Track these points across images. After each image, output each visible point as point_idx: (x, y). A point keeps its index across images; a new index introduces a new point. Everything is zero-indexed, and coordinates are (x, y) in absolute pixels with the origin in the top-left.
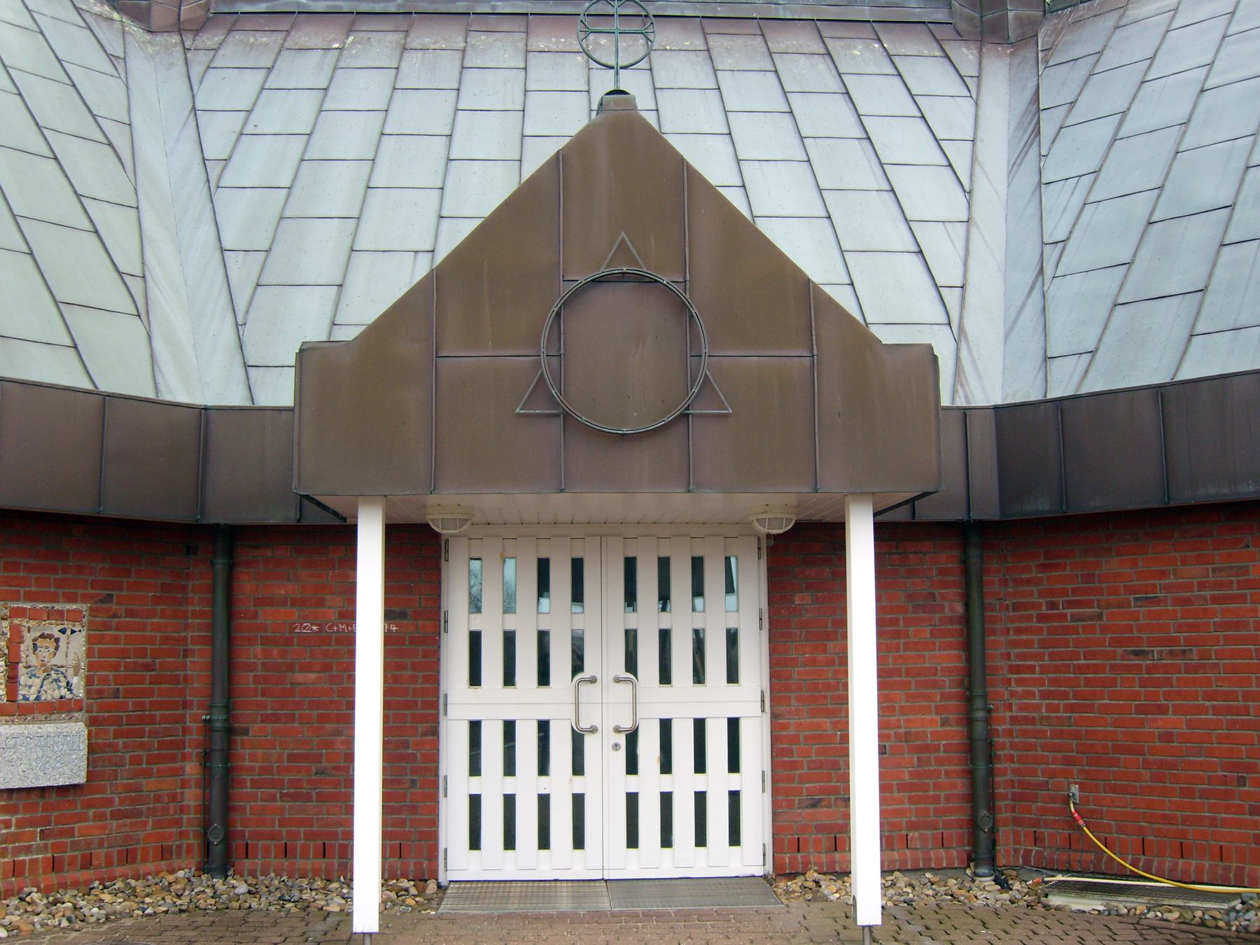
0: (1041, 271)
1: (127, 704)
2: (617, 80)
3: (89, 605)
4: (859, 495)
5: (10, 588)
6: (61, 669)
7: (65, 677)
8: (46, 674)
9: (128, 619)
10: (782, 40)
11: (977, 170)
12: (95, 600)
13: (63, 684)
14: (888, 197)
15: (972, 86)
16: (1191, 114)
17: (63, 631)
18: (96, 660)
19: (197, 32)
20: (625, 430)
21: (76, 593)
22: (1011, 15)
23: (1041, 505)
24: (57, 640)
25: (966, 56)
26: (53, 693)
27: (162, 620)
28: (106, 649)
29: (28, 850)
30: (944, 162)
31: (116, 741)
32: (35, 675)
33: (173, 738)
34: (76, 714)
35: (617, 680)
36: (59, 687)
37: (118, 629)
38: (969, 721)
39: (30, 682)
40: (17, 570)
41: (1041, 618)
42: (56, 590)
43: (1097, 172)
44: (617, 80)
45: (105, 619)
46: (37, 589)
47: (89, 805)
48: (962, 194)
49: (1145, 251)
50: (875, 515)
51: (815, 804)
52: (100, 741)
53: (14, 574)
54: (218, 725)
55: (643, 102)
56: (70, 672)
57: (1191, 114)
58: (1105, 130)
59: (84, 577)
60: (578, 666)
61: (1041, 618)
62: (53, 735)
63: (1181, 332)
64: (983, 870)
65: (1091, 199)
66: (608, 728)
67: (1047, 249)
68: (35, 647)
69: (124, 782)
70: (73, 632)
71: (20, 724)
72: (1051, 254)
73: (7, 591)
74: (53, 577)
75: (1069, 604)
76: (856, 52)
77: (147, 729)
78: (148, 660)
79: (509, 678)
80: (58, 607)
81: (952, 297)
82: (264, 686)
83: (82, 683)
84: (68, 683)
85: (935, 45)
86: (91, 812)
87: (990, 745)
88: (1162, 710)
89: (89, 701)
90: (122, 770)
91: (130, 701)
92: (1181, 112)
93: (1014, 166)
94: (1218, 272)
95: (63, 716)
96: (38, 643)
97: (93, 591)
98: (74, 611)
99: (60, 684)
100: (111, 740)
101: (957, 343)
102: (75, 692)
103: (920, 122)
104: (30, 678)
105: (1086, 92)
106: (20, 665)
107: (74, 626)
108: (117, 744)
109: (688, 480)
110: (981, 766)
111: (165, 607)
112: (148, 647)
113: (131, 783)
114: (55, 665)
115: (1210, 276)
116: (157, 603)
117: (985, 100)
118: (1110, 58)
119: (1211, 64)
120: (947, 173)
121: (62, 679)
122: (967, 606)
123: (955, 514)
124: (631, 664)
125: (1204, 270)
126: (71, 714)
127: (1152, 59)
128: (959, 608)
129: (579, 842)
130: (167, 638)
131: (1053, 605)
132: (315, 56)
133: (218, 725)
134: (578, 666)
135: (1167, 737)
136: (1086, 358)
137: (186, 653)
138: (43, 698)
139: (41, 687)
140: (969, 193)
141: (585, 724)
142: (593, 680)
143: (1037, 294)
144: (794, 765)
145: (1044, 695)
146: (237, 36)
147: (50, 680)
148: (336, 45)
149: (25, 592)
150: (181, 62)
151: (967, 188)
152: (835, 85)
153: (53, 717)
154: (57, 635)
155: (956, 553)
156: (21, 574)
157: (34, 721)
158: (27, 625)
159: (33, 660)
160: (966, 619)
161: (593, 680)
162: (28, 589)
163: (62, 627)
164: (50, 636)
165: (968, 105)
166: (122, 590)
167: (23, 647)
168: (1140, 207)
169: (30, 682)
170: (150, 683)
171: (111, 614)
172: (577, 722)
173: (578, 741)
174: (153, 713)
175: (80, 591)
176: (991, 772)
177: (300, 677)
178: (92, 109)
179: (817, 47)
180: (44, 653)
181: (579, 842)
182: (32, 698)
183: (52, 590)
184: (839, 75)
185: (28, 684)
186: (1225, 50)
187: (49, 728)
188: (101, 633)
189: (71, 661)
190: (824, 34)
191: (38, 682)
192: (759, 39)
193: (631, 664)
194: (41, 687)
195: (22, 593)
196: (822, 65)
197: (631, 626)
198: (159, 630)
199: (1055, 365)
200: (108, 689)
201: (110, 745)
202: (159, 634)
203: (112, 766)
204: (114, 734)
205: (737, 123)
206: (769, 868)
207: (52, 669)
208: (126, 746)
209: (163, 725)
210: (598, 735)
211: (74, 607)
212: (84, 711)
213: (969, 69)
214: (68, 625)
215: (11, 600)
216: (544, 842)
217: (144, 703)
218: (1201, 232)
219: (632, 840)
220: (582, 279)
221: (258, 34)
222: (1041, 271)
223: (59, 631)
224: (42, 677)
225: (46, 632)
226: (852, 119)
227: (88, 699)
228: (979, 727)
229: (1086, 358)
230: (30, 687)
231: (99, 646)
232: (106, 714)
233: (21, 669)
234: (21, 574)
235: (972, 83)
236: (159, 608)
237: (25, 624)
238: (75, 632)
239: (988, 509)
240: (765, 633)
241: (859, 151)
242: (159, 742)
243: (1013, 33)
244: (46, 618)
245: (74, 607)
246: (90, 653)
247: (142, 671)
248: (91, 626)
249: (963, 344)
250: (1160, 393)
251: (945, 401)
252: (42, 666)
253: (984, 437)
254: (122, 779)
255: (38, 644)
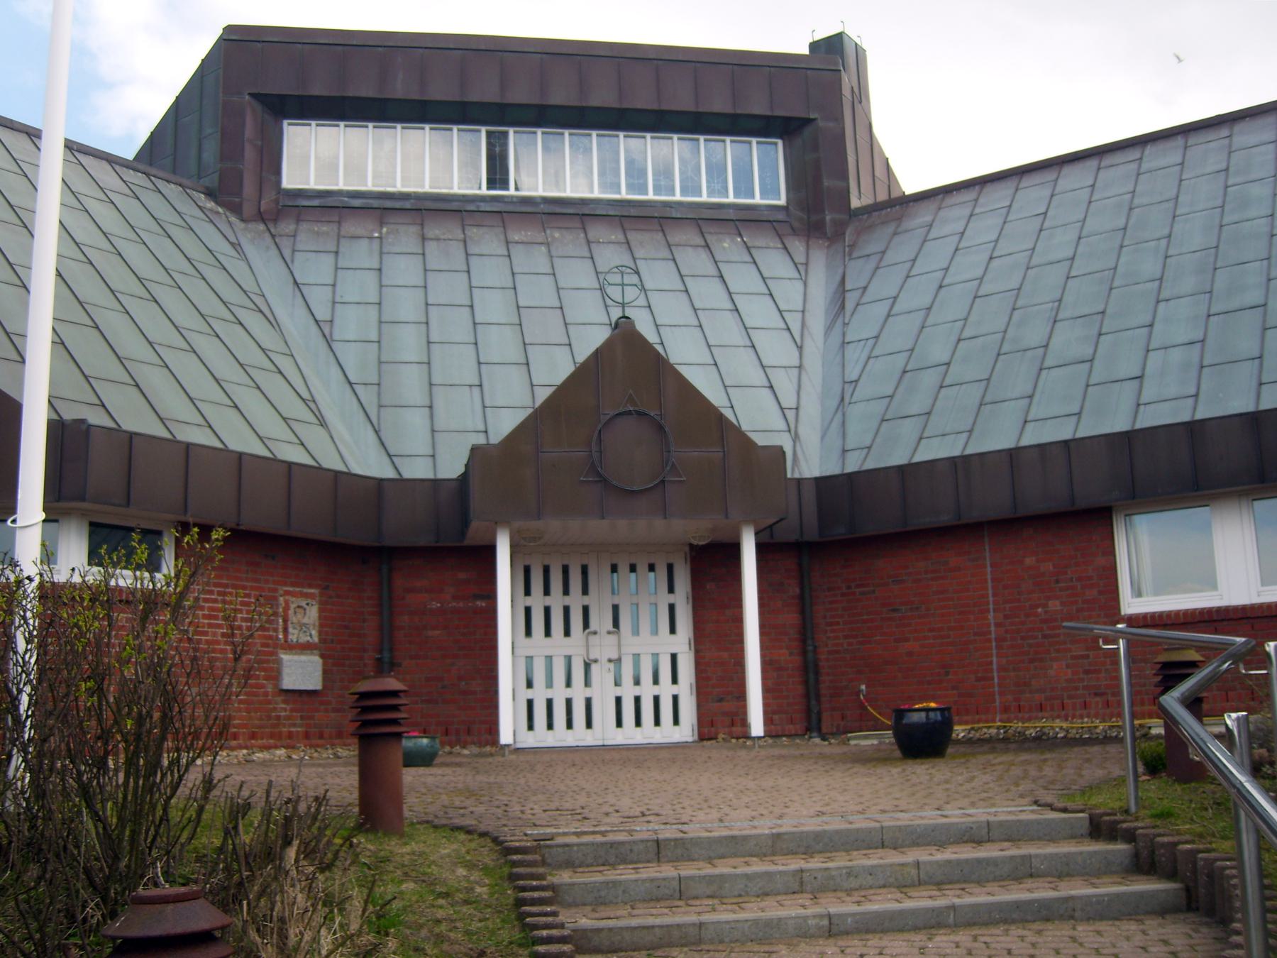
0: (842, 399)
2: (624, 311)
4: (747, 522)
10: (677, 236)
11: (806, 332)
14: (751, 351)
15: (802, 270)
16: (933, 303)
19: (275, 220)
20: (635, 488)
22: (828, 218)
23: (840, 531)
25: (797, 246)
26: (304, 639)
29: (294, 725)
30: (785, 327)
35: (609, 633)
38: (804, 653)
41: (843, 595)
43: (877, 337)
44: (624, 311)
47: (322, 703)
48: (795, 348)
49: (901, 389)
50: (756, 534)
51: (721, 700)
54: (386, 660)
55: (645, 328)
57: (933, 303)
58: (882, 308)
60: (586, 625)
61: (843, 595)
63: (915, 436)
64: (814, 734)
65: (873, 355)
66: (604, 660)
67: (846, 386)
68: (295, 612)
72: (849, 389)
75: (858, 586)
76: (726, 245)
79: (548, 633)
81: (791, 415)
85: (777, 239)
86: (323, 707)
87: (816, 666)
88: (907, 640)
92: (927, 301)
93: (829, 330)
94: (938, 403)
101: (794, 442)
103: (768, 298)
105: (874, 280)
109: (665, 512)
110: (812, 676)
115: (933, 405)
117: (811, 281)
118: (890, 257)
119: (947, 269)
120: (786, 334)
122: (802, 588)
123: (793, 537)
124: (616, 623)
125: (930, 401)
127: (914, 260)
128: (797, 590)
129: (589, 724)
131: (849, 587)
132: (364, 243)
133: (386, 660)
134: (586, 625)
135: (910, 654)
136: (866, 450)
137: (364, 621)
140: (800, 348)
141: (592, 657)
142: (595, 633)
143: (839, 415)
144: (708, 678)
145: (846, 637)
146: (304, 226)
148: (376, 235)
150: (273, 247)
151: (799, 344)
152: (711, 270)
155: (804, 244)
159: (295, 620)
160: (801, 597)
161: (595, 633)
165: (799, 286)
168: (900, 360)
172: (588, 654)
173: (587, 666)
176: (817, 681)
177: (430, 633)
178: (243, 286)
179: (700, 241)
180: (299, 616)
181: (589, 724)
184: (716, 262)
186: (957, 259)
187: (303, 658)
189: (311, 621)
190: (704, 230)
192: (661, 234)
193: (616, 623)
196: (703, 255)
197: (616, 603)
199: (849, 455)
205: (654, 298)
206: (696, 737)
210: (599, 664)
213: (800, 258)
214: (309, 601)
216: (570, 725)
218: (929, 379)
219: (619, 723)
220: (612, 413)
221: (319, 224)
222: (842, 399)
226: (726, 296)
228: (810, 655)
229: (866, 450)
233: (290, 626)
235: (802, 268)
239: (812, 535)
240: (690, 606)
241: (730, 318)
243: (829, 230)
246: (320, 617)
248: (321, 603)
249: (798, 444)
250: (901, 469)
251: (789, 476)
253: (810, 496)
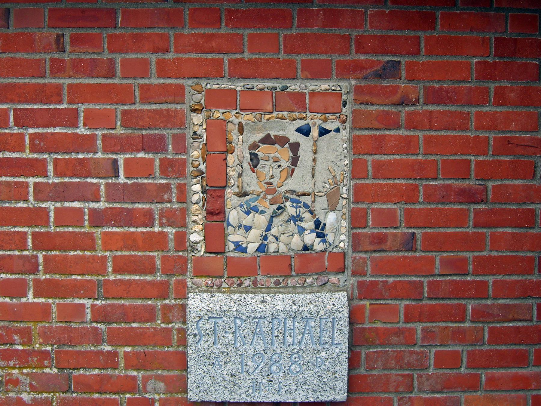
1: (432, 260)
3: (353, 82)
5: (203, 56)
6: (303, 199)
7: (311, 212)
8: (275, 207)
9: (430, 108)
12: (365, 73)
13: (309, 224)
17: (305, 131)
18: (370, 182)
21: (329, 62)
24: (295, 147)
27: (499, 109)
28: (390, 163)
31: (409, 325)
32: (255, 209)
33: (520, 324)
34: (333, 279)
36: (301, 231)
37: (412, 125)
39: (247, 220)
40: (217, 23)
42: (290, 57)
45: (387, 108)
46: (252, 56)
52: (379, 325)
53: (208, 31)
56: (321, 204)
59: (343, 31)
62: (282, 315)
68: (254, 159)
69: (424, 396)
70: (323, 132)
71: (231, 292)
73: (198, 59)
74: (282, 33)
77: (470, 307)
78: (472, 182)
80: (294, 86)
82: (178, 278)
83: (344, 224)
84: (318, 224)
89: (358, 255)
90: (420, 376)
91: (438, 256)
95: (309, 281)
96: (263, 151)
97: (362, 57)
98: (325, 93)
99: (302, 225)
100: (401, 325)
102: (330, 238)
104: (248, 213)
106: (228, 190)
107: (325, 121)
108: (412, 332)
111: (505, 84)
112: (473, 158)
113: (438, 399)
114: (293, 192)
116: (490, 77)
121: (307, 215)
126: (324, 279)
130: (508, 141)
138: (272, 248)
139: (269, 229)
147: (284, 217)
149: (231, 61)
153: (290, 282)
154: (295, 137)
156: (224, 30)
157: (255, 287)
158: (237, 121)
162: (238, 56)
163: (300, 123)
164: (282, 141)
166: (418, 53)
167: (231, 159)
169: (247, 220)
170: (475, 226)
171: (396, 98)
174: (481, 278)
175: (336, 58)
182: (252, 248)
183: (282, 56)
185: (244, 223)
188: (378, 133)
191: (262, 220)
194: (269, 229)
195: (226, 63)
198: (493, 128)
200: (395, 235)
201: (398, 332)
202: (491, 135)
203: (402, 368)
204: (406, 315)
207: (287, 199)
208: (428, 334)
209: (501, 301)
211: (324, 86)
212: (349, 272)
215: (207, 76)
217: (465, 260)
223: (299, 130)
224: (269, 212)
225: (272, 133)
227: (355, 250)
230: (248, 229)
231: (377, 157)
232: (391, 280)
234: (224, 30)
236: (492, 86)
237: (233, 119)
238: (328, 132)
242: (491, 330)
244: (270, 107)
245: (324, 86)
247: (459, 203)
252: (268, 192)
254: (420, 390)
255: (260, 155)
